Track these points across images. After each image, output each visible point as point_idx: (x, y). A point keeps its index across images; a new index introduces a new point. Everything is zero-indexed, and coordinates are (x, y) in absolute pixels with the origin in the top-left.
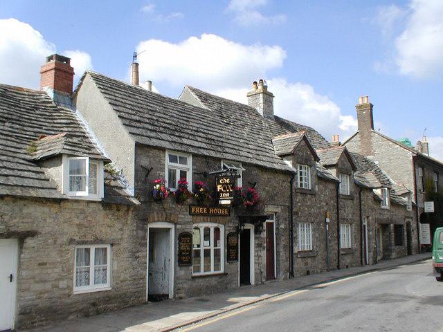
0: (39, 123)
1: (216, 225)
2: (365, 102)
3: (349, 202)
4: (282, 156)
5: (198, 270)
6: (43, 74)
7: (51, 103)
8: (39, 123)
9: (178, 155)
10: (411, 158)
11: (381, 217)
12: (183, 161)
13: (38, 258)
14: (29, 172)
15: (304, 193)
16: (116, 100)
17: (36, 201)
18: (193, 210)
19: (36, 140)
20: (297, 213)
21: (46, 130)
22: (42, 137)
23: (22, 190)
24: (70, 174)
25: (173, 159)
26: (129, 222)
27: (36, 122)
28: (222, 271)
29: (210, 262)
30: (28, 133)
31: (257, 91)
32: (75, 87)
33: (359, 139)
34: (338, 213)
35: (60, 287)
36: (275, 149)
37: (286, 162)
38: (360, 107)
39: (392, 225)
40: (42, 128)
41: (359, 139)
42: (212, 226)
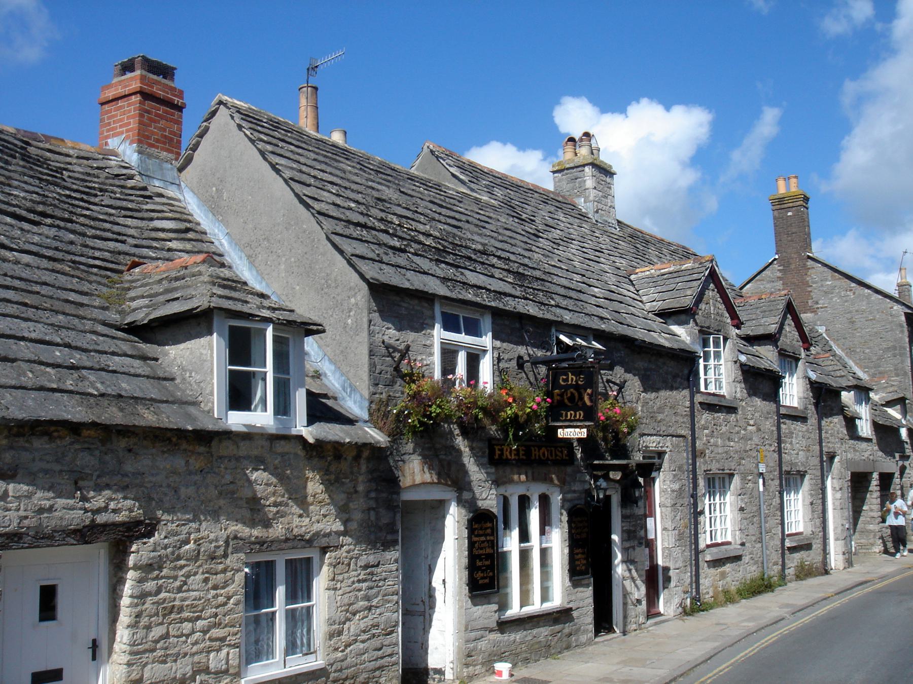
0: (116, 228)
1: (521, 490)
2: (794, 189)
3: (798, 426)
4: (667, 315)
5: (504, 606)
6: (106, 107)
7: (131, 177)
8: (116, 228)
9: (462, 314)
10: (903, 318)
11: (857, 457)
12: (473, 329)
13: (163, 595)
14: (123, 356)
15: (716, 406)
16: (301, 171)
17: (156, 437)
18: (498, 452)
19: (121, 272)
20: (703, 453)
21: (136, 246)
22: (135, 265)
23: (121, 410)
24: (232, 363)
25: (451, 324)
26: (361, 488)
27: (107, 226)
28: (557, 601)
29: (663, 549)
30: (97, 254)
31: (579, 161)
32: (187, 140)
33: (779, 274)
34: (780, 451)
35: (212, 666)
36: (644, 299)
37: (675, 328)
38: (780, 203)
39: (875, 476)
40: (124, 242)
41: (779, 274)
42: (535, 492)
